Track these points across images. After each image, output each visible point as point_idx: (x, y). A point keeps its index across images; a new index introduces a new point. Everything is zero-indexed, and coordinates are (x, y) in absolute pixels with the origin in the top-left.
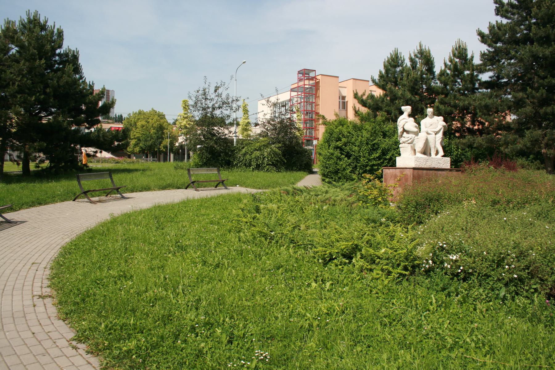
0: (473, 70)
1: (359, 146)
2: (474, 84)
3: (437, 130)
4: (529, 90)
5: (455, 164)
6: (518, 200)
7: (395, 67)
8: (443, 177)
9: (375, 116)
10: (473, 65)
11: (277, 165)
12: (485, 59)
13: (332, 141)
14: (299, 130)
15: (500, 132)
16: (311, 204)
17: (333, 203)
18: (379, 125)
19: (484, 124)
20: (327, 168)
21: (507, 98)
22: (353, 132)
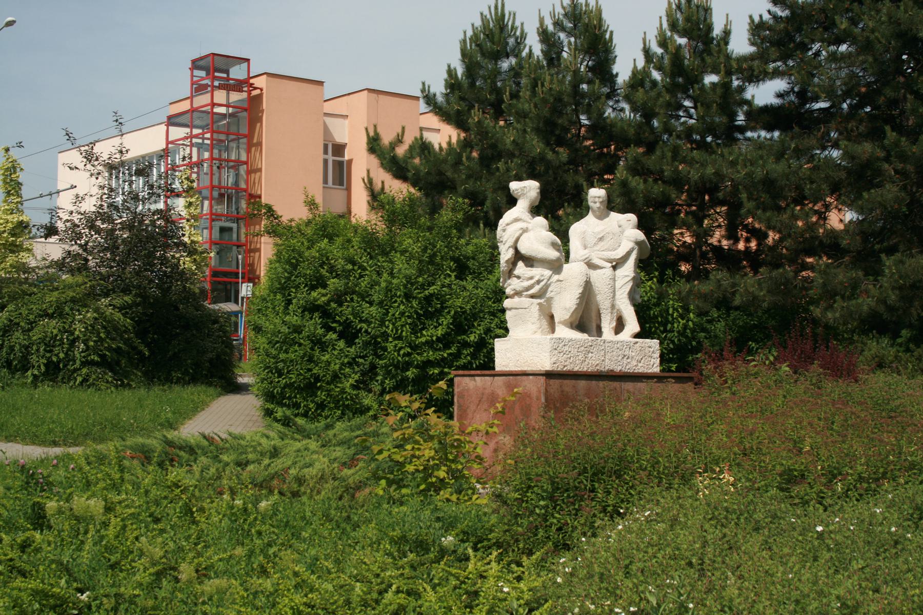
0: (729, 73)
1: (381, 304)
2: (732, 116)
3: (619, 253)
4: (891, 135)
5: (679, 360)
6: (859, 468)
7: (497, 56)
8: (637, 401)
9: (434, 209)
10: (728, 57)
11: (118, 363)
12: (763, 40)
13: (297, 287)
14: (191, 250)
15: (810, 260)
16: (221, 493)
17: (295, 486)
18: (446, 237)
19: (766, 236)
20: (280, 375)
21: (829, 160)
22: (364, 260)
